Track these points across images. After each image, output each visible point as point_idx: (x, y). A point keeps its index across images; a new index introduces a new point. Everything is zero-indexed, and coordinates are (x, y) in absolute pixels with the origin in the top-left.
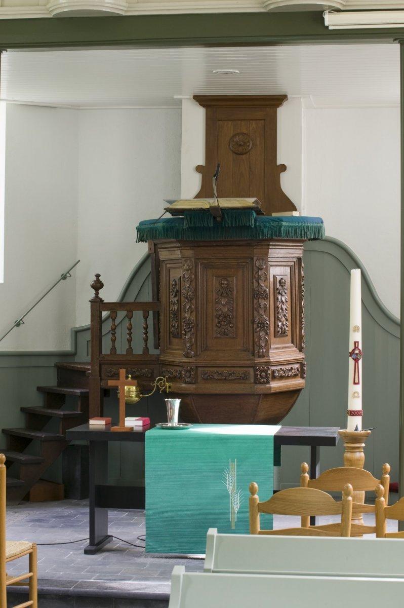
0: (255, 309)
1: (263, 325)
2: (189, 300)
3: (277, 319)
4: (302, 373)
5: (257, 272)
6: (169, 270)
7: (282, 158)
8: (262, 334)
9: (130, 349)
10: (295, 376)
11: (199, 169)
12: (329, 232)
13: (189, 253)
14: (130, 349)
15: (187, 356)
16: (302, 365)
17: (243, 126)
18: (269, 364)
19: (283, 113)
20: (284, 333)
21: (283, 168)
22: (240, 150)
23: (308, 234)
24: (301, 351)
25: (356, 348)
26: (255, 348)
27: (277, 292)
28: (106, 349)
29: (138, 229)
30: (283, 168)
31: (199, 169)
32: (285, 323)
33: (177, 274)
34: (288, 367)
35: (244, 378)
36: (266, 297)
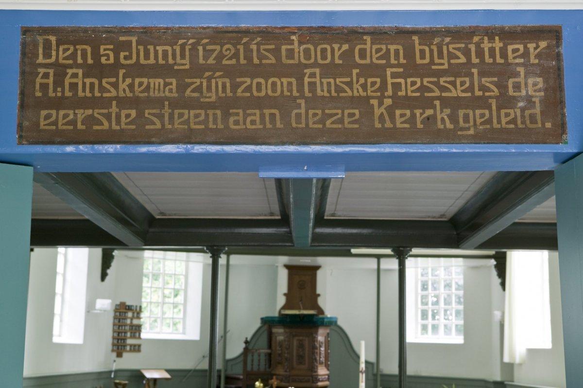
0: (313, 353)
1: (316, 359)
2: (287, 349)
3: (320, 357)
4: (328, 379)
5: (314, 340)
6: (276, 337)
7: (318, 291)
8: (316, 363)
9: (252, 368)
10: (326, 381)
11: (285, 294)
12: (339, 323)
13: (287, 330)
14: (252, 368)
15: (286, 371)
16: (329, 376)
17: (303, 282)
18: (318, 375)
19: (320, 274)
20: (322, 363)
21: (319, 295)
22: (302, 286)
23: (332, 323)
24: (328, 370)
25: (362, 369)
26: (313, 369)
27: (320, 346)
28: (249, 368)
29: (262, 319)
30: (319, 295)
31: (285, 294)
32: (323, 359)
33: (281, 338)
34: (303, 378)
35: (308, 381)
36: (317, 349)
